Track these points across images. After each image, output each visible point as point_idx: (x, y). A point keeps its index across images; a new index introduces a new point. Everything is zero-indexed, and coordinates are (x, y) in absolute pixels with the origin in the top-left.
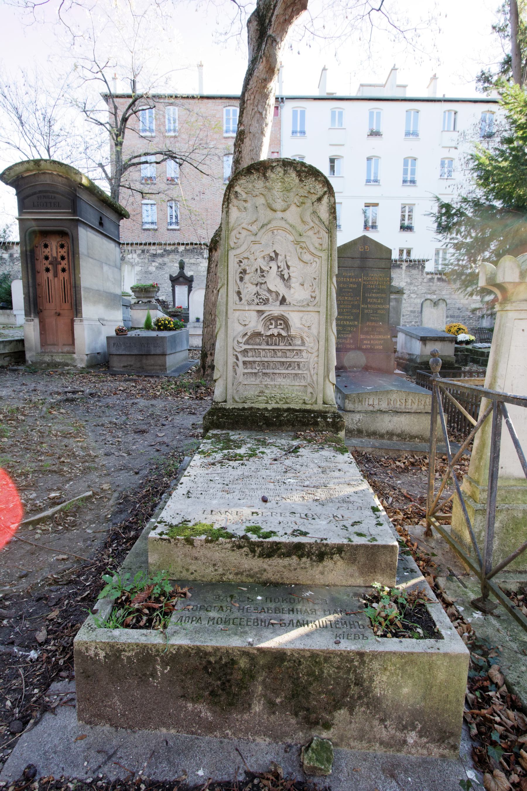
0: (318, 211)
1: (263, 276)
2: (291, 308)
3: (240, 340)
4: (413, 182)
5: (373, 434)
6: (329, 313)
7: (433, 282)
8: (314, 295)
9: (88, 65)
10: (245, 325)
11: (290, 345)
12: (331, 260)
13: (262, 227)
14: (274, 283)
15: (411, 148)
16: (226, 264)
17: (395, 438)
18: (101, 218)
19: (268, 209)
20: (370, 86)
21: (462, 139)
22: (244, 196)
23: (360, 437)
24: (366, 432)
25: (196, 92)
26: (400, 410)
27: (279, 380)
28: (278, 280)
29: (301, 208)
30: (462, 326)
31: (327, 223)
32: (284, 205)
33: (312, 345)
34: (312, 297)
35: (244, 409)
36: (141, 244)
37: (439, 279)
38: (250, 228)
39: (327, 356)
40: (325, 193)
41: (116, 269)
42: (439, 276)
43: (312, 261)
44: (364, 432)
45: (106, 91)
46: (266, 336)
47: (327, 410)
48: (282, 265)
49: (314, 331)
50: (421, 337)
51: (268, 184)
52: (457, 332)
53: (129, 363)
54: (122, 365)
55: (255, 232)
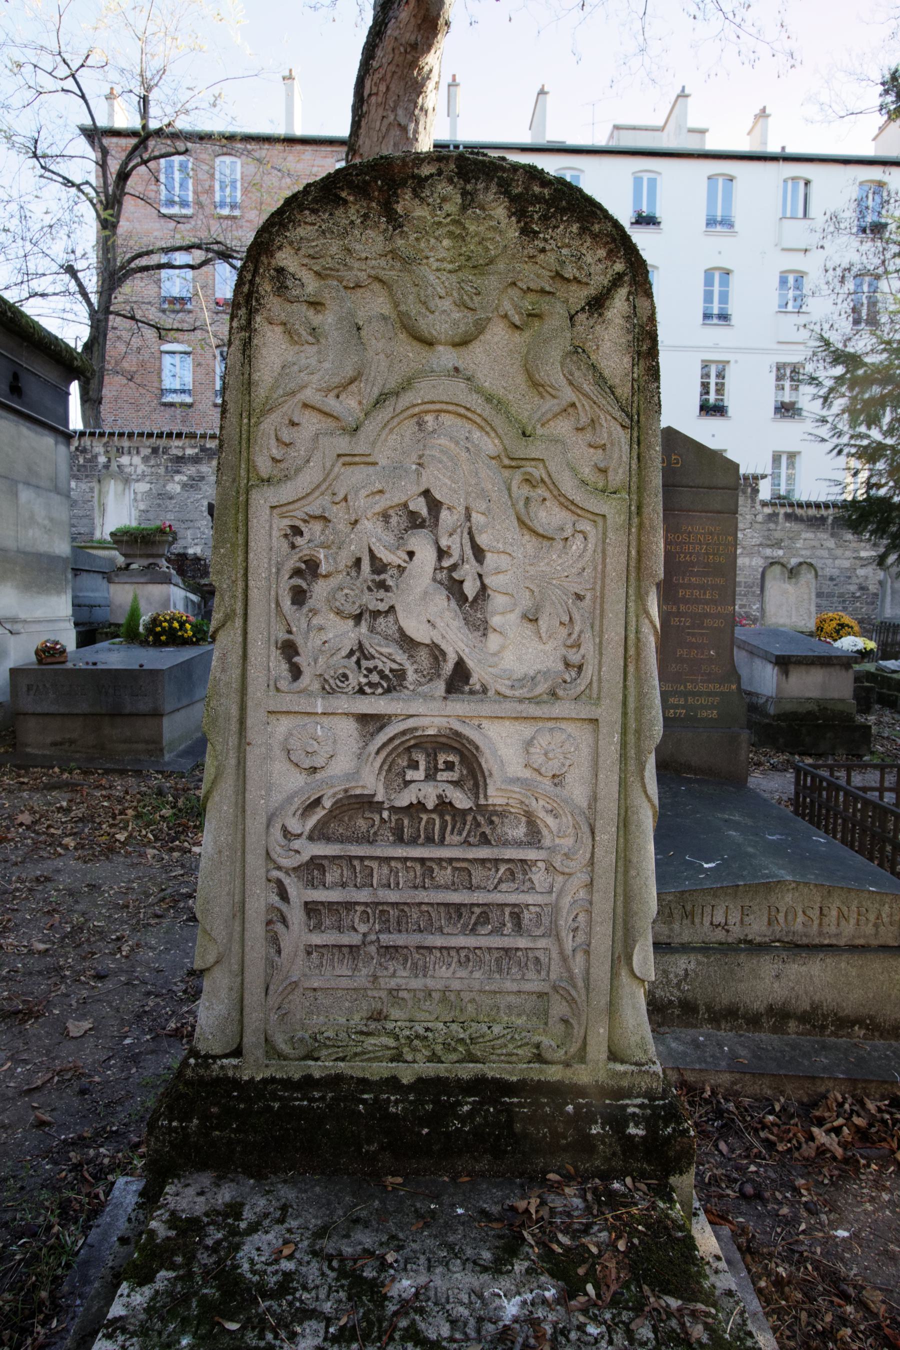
0: (590, 346)
1: (382, 586)
2: (486, 709)
3: (294, 825)
4: (724, 317)
5: (729, 1015)
6: (632, 725)
7: (776, 523)
8: (575, 658)
9: (47, 62)
10: (314, 770)
11: (485, 840)
12: (641, 526)
13: (380, 401)
14: (426, 614)
15: (718, 250)
16: (241, 537)
17: (792, 1025)
18: (16, 377)
19: (403, 336)
20: (634, 128)
21: (832, 229)
22: (311, 285)
23: (688, 1025)
24: (709, 1009)
25: (280, 130)
26: (805, 941)
27: (443, 972)
28: (441, 602)
29: (527, 334)
30: (847, 620)
31: (624, 391)
32: (461, 320)
33: (567, 842)
34: (567, 665)
35: (308, 1082)
36: (150, 435)
37: (788, 516)
38: (331, 403)
39: (626, 883)
40: (617, 281)
41: (57, 498)
42: (789, 510)
43: (568, 532)
44: (702, 1009)
45: (88, 122)
46: (393, 809)
47: (625, 1083)
48: (455, 544)
49: (577, 791)
50: (777, 657)
51: (400, 242)
52: (838, 632)
53: (68, 736)
54: (49, 740)
55: (351, 421)
